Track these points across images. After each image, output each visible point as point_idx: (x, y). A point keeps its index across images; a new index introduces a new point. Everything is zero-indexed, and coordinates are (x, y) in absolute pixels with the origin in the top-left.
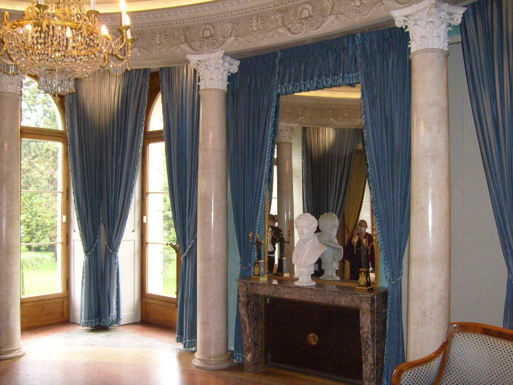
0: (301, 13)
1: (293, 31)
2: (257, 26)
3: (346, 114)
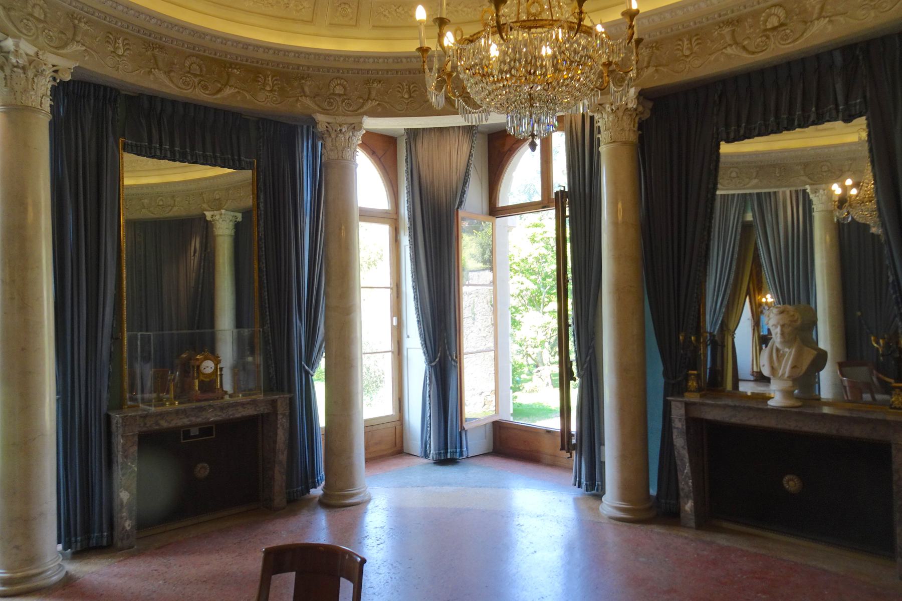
0: (765, 21)
1: (752, 49)
2: (691, 49)
3: (734, 175)
